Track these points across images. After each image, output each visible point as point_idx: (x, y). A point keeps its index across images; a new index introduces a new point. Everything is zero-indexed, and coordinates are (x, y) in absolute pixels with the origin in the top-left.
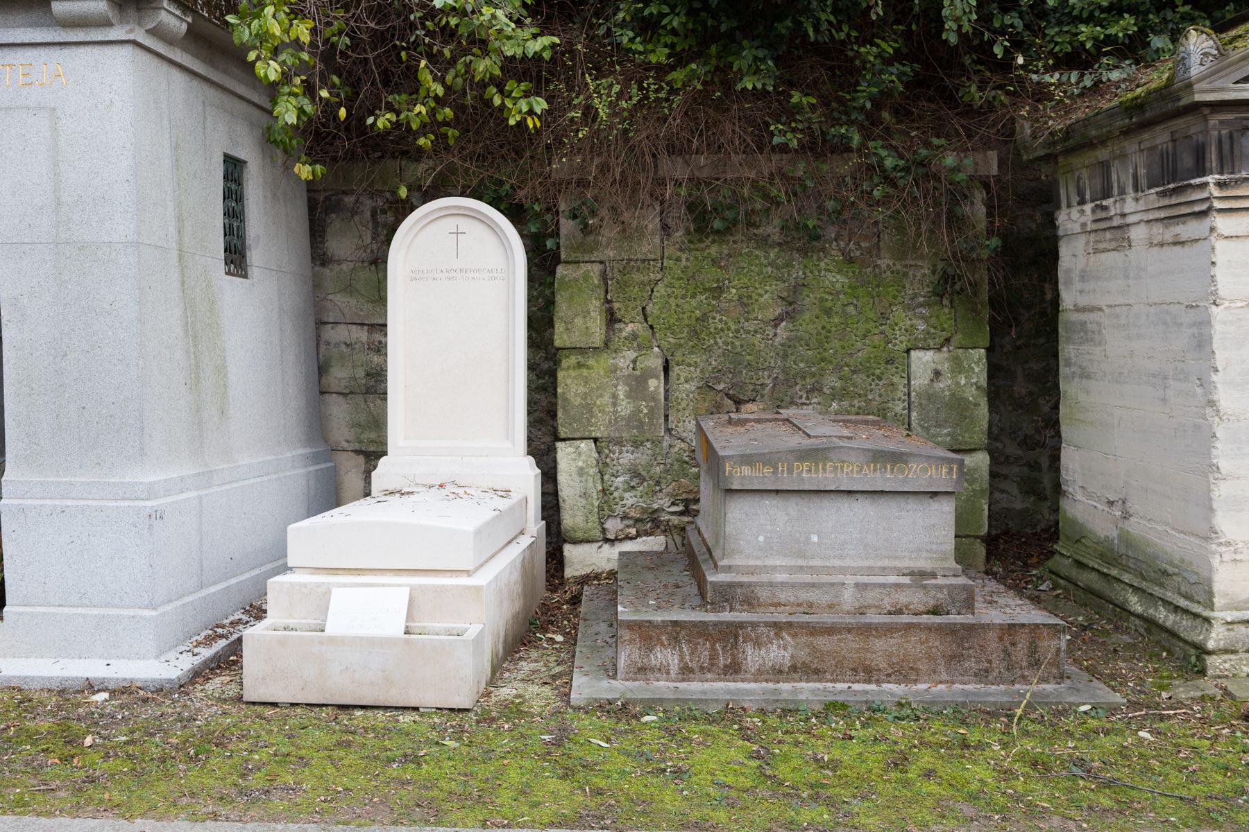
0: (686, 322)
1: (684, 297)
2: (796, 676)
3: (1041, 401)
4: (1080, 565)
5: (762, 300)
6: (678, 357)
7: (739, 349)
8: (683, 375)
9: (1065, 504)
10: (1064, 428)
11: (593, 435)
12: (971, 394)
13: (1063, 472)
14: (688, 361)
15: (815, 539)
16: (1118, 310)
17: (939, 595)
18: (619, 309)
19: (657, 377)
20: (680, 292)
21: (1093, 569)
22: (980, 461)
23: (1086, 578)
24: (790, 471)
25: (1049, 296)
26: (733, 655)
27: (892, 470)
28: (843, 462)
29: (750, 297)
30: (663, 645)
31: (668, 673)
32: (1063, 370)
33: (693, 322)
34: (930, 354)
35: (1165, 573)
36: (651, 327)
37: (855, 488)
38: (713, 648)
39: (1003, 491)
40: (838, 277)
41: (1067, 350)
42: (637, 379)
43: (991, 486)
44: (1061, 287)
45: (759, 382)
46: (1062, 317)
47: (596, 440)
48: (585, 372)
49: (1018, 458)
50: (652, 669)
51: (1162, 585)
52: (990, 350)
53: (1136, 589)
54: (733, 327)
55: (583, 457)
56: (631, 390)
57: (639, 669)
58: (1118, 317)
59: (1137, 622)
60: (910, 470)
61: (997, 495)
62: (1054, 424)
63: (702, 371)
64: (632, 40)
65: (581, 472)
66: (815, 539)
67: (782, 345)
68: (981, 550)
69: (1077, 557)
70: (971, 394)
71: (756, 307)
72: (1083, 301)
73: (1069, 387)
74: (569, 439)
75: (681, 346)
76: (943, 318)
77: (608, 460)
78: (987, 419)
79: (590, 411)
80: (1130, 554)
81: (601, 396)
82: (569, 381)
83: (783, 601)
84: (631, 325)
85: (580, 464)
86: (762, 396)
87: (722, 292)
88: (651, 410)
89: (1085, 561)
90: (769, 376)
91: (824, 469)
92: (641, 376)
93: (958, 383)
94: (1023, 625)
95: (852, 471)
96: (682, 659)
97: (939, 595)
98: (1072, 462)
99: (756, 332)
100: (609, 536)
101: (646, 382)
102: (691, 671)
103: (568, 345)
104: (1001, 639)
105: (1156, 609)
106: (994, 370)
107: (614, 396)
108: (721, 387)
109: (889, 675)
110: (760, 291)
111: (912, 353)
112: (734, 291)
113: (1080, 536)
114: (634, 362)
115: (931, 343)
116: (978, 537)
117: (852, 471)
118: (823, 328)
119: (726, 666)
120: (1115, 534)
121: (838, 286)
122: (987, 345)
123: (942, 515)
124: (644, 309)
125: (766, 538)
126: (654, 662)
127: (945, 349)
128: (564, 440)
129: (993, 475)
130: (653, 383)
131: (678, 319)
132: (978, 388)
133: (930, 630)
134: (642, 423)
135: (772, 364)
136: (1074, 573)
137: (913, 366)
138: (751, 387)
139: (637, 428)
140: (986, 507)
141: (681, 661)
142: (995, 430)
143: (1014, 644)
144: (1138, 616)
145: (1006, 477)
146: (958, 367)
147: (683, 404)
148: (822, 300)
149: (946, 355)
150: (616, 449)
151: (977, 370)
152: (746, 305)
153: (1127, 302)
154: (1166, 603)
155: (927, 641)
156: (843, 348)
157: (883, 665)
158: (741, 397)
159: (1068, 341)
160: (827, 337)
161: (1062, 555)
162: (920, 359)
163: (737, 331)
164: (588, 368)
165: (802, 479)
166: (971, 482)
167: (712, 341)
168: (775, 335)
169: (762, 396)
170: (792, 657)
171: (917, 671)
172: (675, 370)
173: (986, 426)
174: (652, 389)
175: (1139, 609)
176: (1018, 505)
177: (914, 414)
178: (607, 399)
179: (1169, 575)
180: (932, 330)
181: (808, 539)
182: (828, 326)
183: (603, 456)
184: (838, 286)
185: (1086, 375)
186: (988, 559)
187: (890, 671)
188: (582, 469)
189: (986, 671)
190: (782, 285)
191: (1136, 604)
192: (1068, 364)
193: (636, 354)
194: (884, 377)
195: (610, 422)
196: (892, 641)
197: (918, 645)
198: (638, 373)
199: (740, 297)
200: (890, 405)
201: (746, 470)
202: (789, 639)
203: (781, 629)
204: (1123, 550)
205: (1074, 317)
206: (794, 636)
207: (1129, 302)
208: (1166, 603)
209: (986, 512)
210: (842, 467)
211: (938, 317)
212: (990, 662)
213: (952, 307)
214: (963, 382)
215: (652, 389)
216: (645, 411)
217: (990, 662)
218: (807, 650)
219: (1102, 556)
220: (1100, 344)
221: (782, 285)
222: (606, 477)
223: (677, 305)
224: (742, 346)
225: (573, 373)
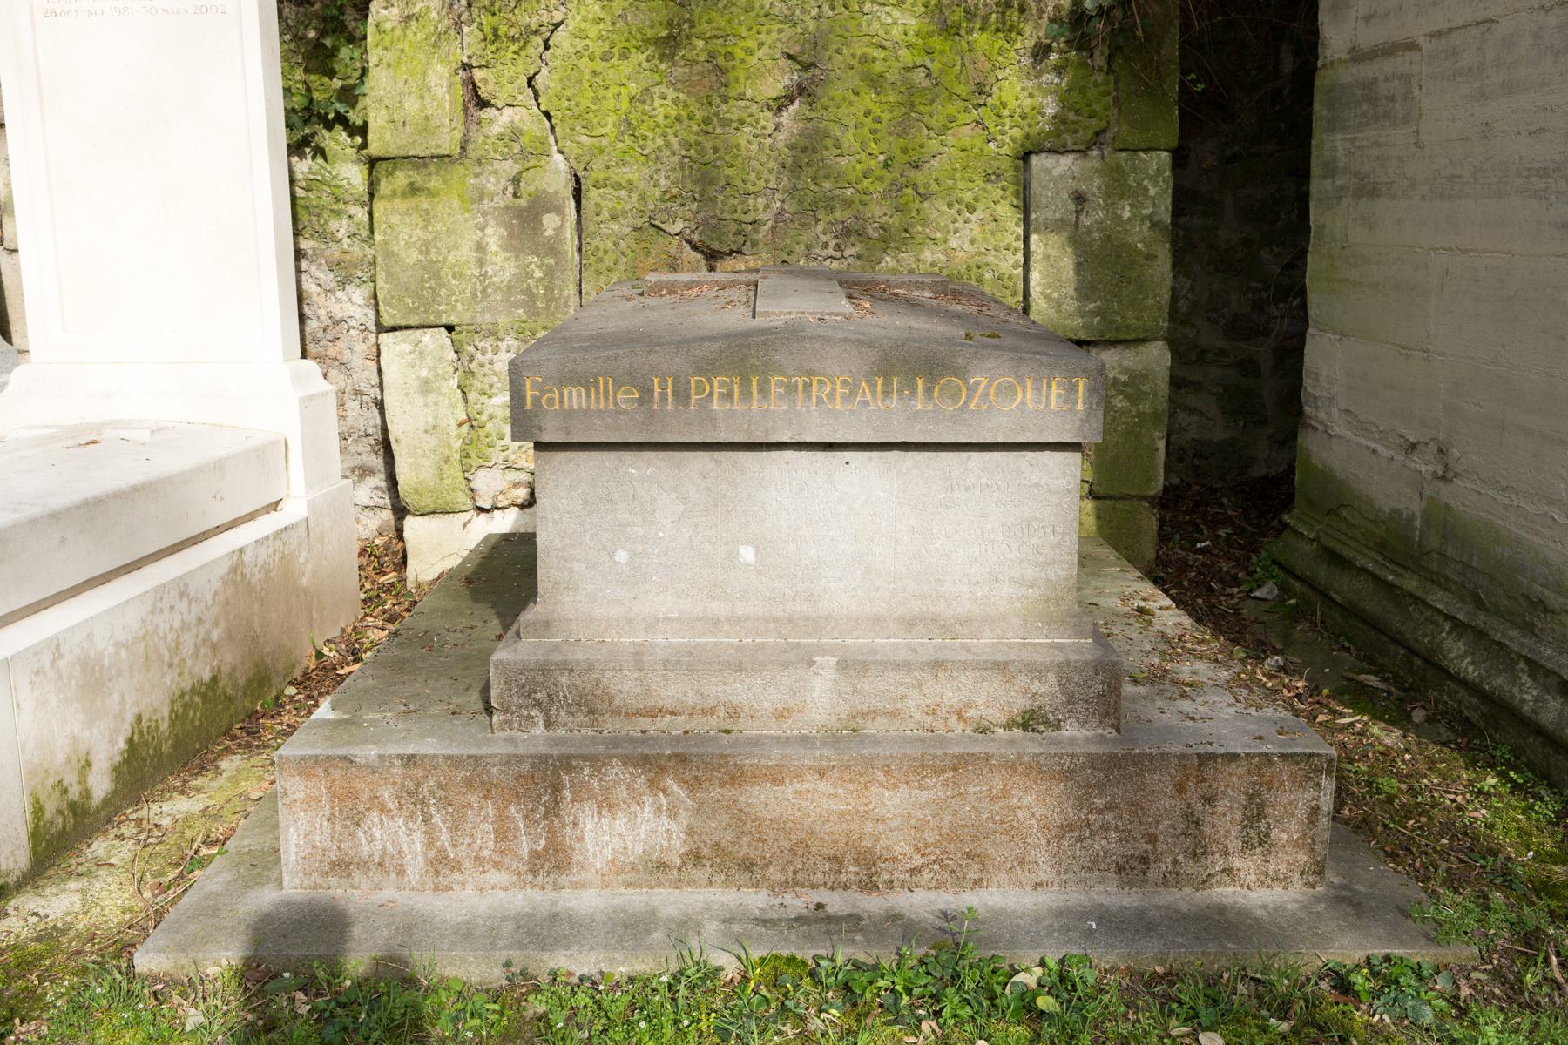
0: (611, 104)
1: (606, 57)
2: (701, 874)
3: (1265, 255)
4: (1337, 560)
5: (753, 60)
6: (598, 172)
7: (710, 156)
8: (607, 205)
9: (1309, 442)
10: (1313, 298)
11: (444, 321)
12: (1140, 237)
13: (1308, 383)
14: (615, 178)
15: (748, 554)
16: (1456, 39)
17: (1037, 687)
18: (485, 81)
19: (559, 210)
20: (598, 48)
21: (1363, 570)
22: (1156, 357)
23: (1344, 587)
24: (682, 397)
25: (1287, 65)
26: (551, 831)
27: (929, 391)
28: (811, 373)
29: (730, 56)
30: (383, 809)
31: (401, 872)
32: (1318, 186)
33: (625, 105)
34: (1067, 161)
35: (1540, 605)
36: (547, 115)
37: (838, 438)
38: (501, 817)
39: (1192, 411)
40: (896, 13)
41: (1332, 145)
42: (520, 213)
43: (1171, 400)
44: (1324, 17)
45: (749, 218)
46: (1322, 81)
47: (450, 328)
48: (424, 202)
49: (1222, 353)
50: (364, 865)
51: (1528, 629)
52: (1179, 159)
53: (1459, 627)
54: (699, 115)
55: (429, 361)
56: (511, 236)
57: (333, 864)
58: (1455, 53)
59: (1462, 694)
60: (972, 391)
61: (1182, 417)
62: (1292, 292)
63: (642, 198)
64: (1461, 657)
65: (426, 387)
66: (748, 554)
67: (792, 147)
68: (1149, 521)
69: (1331, 544)
70: (1140, 237)
71: (741, 74)
72: (1370, 37)
73: (1333, 218)
74: (401, 328)
75: (602, 150)
76: (1092, 93)
77: (473, 366)
78: (1168, 283)
79: (436, 275)
80: (1450, 551)
81: (456, 246)
82: (395, 220)
83: (668, 703)
84: (507, 112)
85: (424, 373)
86: (754, 244)
87: (678, 45)
88: (550, 272)
89: (1347, 553)
90: (767, 207)
91: (764, 392)
92: (529, 209)
93: (1117, 218)
94: (1234, 757)
95: (832, 395)
96: (431, 842)
97: (1037, 687)
98: (1327, 362)
99: (741, 121)
100: (481, 504)
101: (537, 219)
102: (456, 866)
103: (394, 152)
104: (1181, 789)
105: (1514, 679)
106: (1183, 199)
107: (480, 247)
108: (678, 226)
109: (915, 871)
110: (750, 43)
111: (1034, 160)
112: (700, 43)
113: (1335, 501)
114: (516, 181)
115: (1069, 140)
116: (1145, 498)
117: (832, 395)
118: (867, 113)
119: (535, 854)
120: (1416, 507)
121: (896, 32)
122: (1174, 143)
123: (1062, 476)
124: (530, 80)
125: (633, 555)
126: (365, 849)
127: (1095, 153)
128: (394, 329)
129: (1176, 382)
130: (550, 222)
131: (596, 100)
132: (1154, 225)
133: (1013, 768)
134: (532, 297)
135: (772, 184)
136: (1323, 573)
137: (1034, 185)
138: (733, 227)
139: (524, 304)
140: (1162, 445)
141: (430, 844)
142: (1183, 306)
143: (1209, 800)
144: (1465, 683)
145: (1197, 387)
146: (1119, 185)
147: (608, 261)
148: (864, 59)
149: (1097, 164)
150: (487, 344)
151: (1152, 191)
152: (722, 71)
153: (1480, 16)
154: (1534, 667)
155: (1005, 793)
156: (905, 151)
157: (902, 848)
158: (715, 246)
159: (1332, 127)
160: (873, 131)
161: (1296, 532)
162: (1048, 171)
163: (707, 121)
164: (431, 194)
165: (711, 418)
166: (1133, 399)
167: (660, 142)
168: (777, 127)
169: (754, 244)
170: (690, 832)
171: (980, 858)
172: (592, 196)
173: (1166, 296)
174: (549, 232)
175: (1469, 670)
176: (1218, 434)
177: (1035, 276)
178: (465, 252)
179: (1546, 610)
180: (1072, 116)
181: (732, 556)
182: (876, 110)
183: (465, 358)
184: (896, 32)
185: (1367, 189)
186: (1163, 538)
187: (918, 861)
188: (427, 382)
189: (1144, 860)
190: (792, 32)
191: (1460, 658)
192: (1330, 171)
193: (517, 168)
194: (980, 206)
195: (474, 295)
196: (923, 796)
197: (986, 804)
198: (523, 202)
199: (712, 56)
200: (990, 259)
201: (575, 397)
202: (682, 793)
203: (662, 769)
204: (1433, 542)
205: (1350, 74)
206: (694, 785)
207: (1488, 14)
208: (1534, 667)
209: (1162, 454)
210: (807, 386)
211: (1083, 90)
212: (1152, 839)
213: (1110, 71)
214: (1127, 214)
215: (549, 232)
216: (538, 274)
217: (1152, 839)
218: (725, 818)
219: (1382, 547)
220: (1406, 120)
221: (792, 32)
222: (471, 396)
223: (594, 73)
224: (715, 150)
225: (398, 203)
